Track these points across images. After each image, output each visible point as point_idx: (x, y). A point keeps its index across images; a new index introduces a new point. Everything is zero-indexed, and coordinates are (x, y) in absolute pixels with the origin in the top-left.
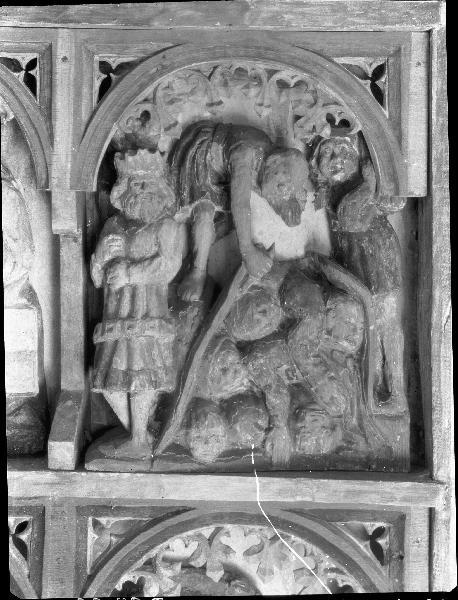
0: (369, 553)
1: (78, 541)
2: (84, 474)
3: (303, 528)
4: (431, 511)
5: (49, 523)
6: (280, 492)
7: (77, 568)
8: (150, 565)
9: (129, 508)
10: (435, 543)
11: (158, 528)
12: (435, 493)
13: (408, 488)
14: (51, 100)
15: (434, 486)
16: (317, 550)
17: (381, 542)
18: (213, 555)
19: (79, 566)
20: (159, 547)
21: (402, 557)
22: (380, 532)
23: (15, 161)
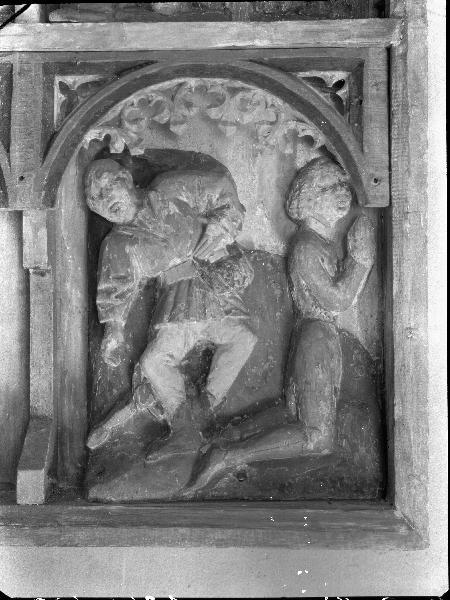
0: (330, 102)
1: (45, 100)
2: (48, 25)
3: (264, 78)
4: (389, 50)
5: (16, 78)
6: (239, 36)
7: (44, 122)
8: (118, 123)
9: (94, 64)
10: (393, 80)
11: (123, 81)
12: (391, 29)
13: (364, 24)
14: (110, 411)
15: (390, 20)
16: (279, 102)
17: (340, 93)
18: (176, 110)
19: (46, 122)
20: (124, 101)
21: (361, 102)
22: (340, 84)
23: (285, 6)
